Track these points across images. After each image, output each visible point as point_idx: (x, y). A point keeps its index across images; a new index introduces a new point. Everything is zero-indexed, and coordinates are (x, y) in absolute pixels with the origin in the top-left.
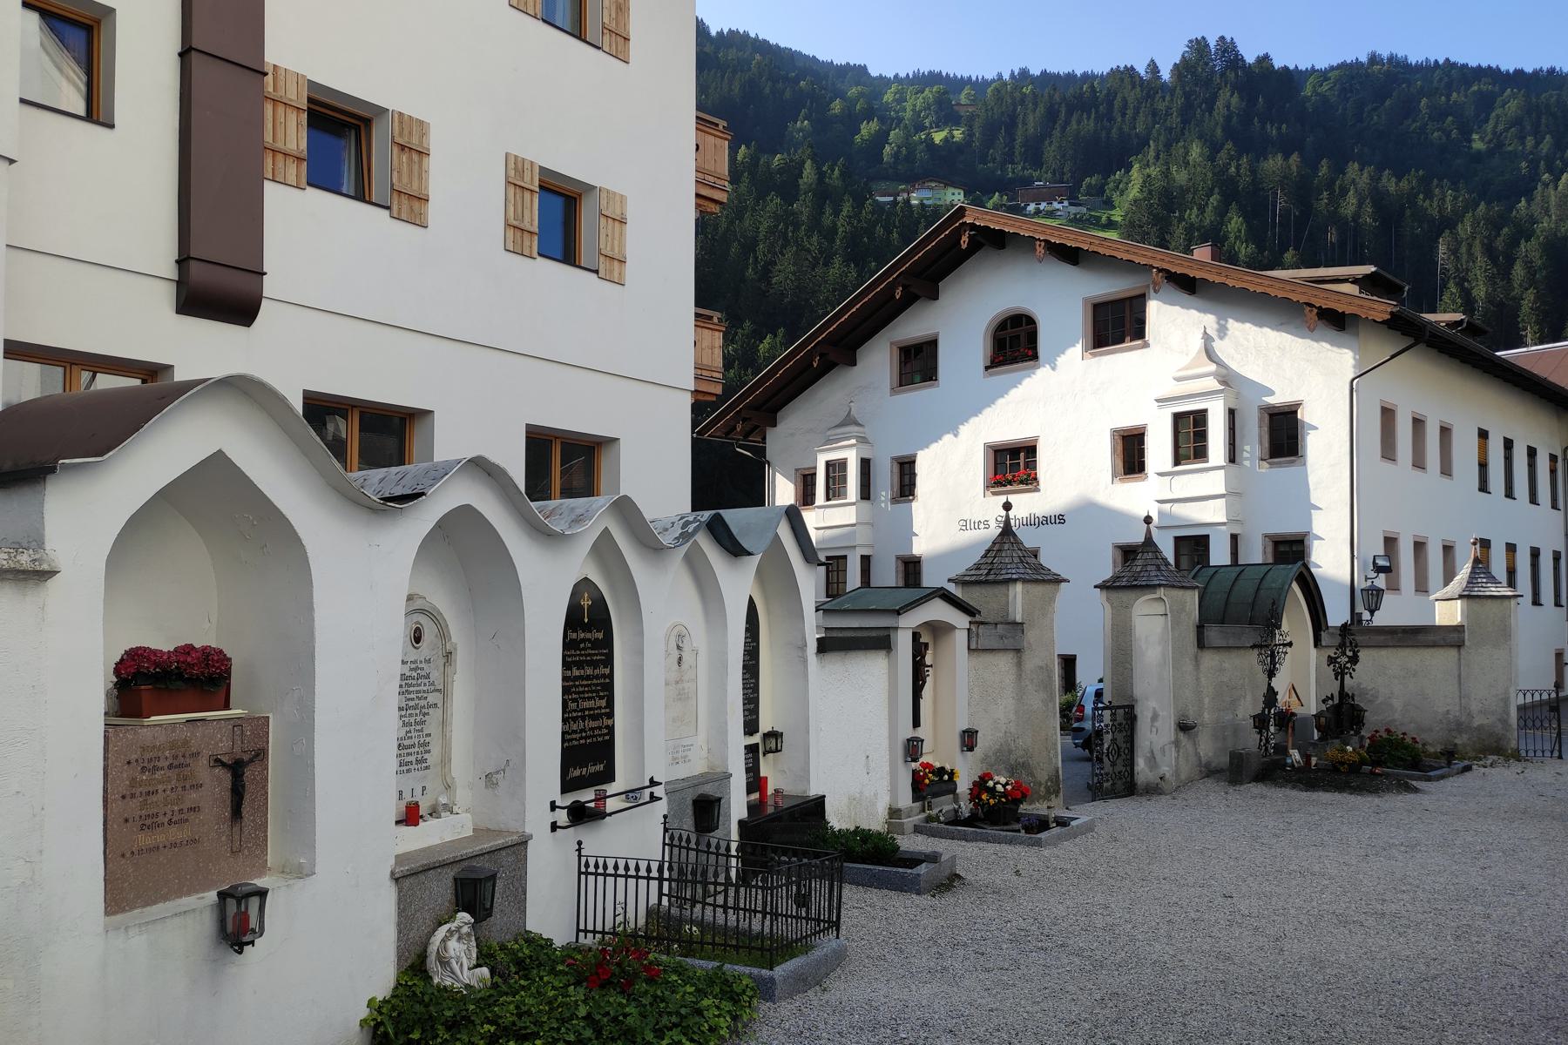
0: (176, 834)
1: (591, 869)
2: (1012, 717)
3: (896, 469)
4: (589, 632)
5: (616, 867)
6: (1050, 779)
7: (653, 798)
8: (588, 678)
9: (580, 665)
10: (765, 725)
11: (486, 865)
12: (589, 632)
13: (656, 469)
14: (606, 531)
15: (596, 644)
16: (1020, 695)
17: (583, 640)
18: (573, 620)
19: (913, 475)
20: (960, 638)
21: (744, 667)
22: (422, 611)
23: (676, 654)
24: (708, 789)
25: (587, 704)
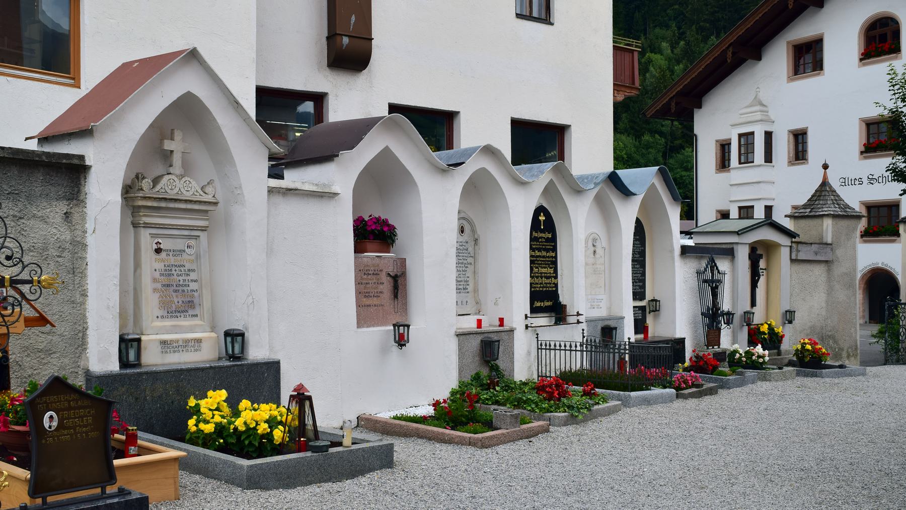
0: (375, 301)
1: (544, 347)
2: (824, 305)
3: (792, 137)
4: (544, 231)
5: (555, 345)
6: (850, 347)
7: (578, 322)
8: (544, 257)
9: (539, 250)
10: (649, 296)
11: (495, 337)
12: (544, 231)
13: (592, 148)
14: (551, 181)
15: (548, 240)
16: (830, 290)
17: (541, 238)
18: (535, 225)
19: (805, 143)
20: (784, 253)
21: (633, 261)
22: (464, 218)
23: (592, 249)
24: (612, 324)
25: (544, 270)
